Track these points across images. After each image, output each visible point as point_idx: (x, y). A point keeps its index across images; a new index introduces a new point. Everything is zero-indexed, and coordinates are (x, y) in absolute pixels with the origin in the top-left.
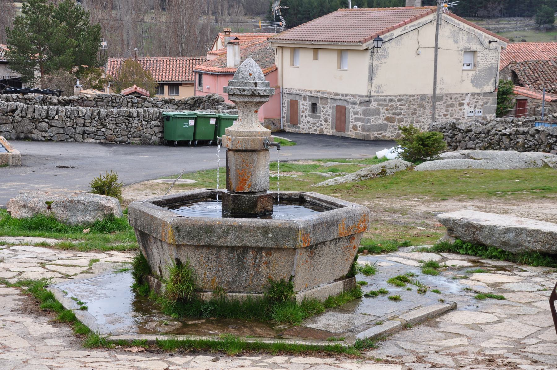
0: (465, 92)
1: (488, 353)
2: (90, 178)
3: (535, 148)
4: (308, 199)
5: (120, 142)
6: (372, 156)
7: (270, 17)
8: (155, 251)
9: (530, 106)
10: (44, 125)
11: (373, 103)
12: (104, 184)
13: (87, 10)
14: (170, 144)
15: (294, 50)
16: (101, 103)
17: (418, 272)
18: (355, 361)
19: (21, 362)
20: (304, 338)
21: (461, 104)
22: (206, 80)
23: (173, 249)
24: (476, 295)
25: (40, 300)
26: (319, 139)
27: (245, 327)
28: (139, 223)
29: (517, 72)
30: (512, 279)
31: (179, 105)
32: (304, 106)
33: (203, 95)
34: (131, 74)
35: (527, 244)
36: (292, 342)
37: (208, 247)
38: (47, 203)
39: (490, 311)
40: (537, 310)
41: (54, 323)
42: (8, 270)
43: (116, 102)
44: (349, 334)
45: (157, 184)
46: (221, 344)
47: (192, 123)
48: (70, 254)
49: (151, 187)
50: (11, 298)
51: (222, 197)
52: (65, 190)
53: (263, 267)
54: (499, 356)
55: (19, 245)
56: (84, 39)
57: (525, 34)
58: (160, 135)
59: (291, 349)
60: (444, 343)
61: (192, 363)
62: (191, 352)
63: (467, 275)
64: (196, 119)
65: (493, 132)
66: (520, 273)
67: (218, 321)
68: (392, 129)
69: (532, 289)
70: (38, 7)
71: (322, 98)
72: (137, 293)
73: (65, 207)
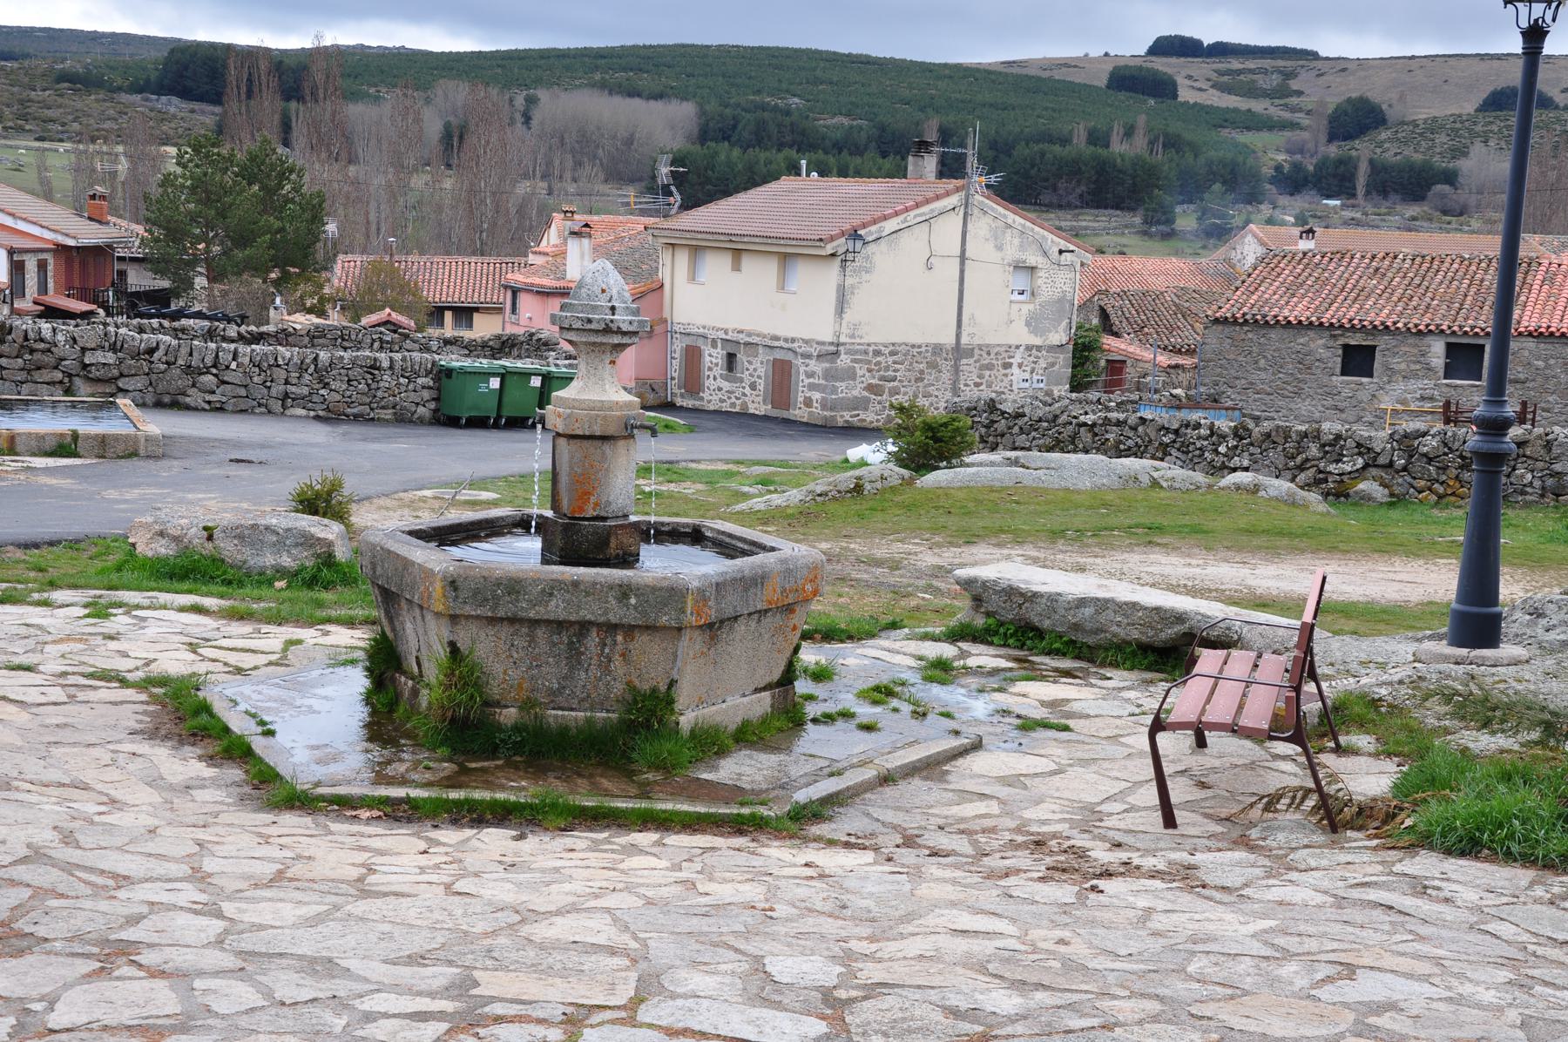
0: (1014, 342)
1: (1034, 829)
2: (291, 484)
3: (1137, 452)
4: (708, 534)
5: (356, 416)
6: (839, 458)
7: (652, 187)
8: (408, 625)
9: (1130, 373)
10: (208, 379)
11: (843, 357)
12: (318, 495)
13: (299, 163)
14: (453, 422)
15: (696, 250)
16: (321, 341)
17: (914, 678)
18: (788, 843)
19: (143, 831)
20: (692, 798)
21: (1008, 366)
22: (525, 301)
23: (445, 621)
24: (1019, 722)
25: (185, 715)
26: (739, 421)
27: (580, 775)
28: (379, 570)
29: (1109, 310)
30: (1086, 693)
31: (471, 348)
32: (713, 358)
33: (519, 331)
34: (383, 287)
35: (1114, 628)
36: (669, 806)
37: (512, 620)
38: (205, 528)
39: (1042, 752)
40: (1127, 751)
41: (210, 759)
42: (125, 655)
43: (350, 340)
44: (781, 792)
45: (423, 500)
46: (531, 806)
47: (495, 383)
48: (247, 628)
49: (411, 505)
50: (132, 708)
51: (543, 527)
52: (245, 505)
53: (617, 662)
54: (1054, 836)
55: (148, 608)
56: (292, 218)
57: (1124, 240)
58: (432, 405)
59: (666, 820)
60: (956, 811)
61: (474, 842)
62: (472, 820)
63: (1004, 684)
64: (504, 376)
65: (1064, 418)
66: (1100, 683)
67: (528, 764)
68: (878, 407)
69: (1121, 713)
70: (207, 156)
71: (747, 344)
72: (373, 706)
73: (241, 537)
